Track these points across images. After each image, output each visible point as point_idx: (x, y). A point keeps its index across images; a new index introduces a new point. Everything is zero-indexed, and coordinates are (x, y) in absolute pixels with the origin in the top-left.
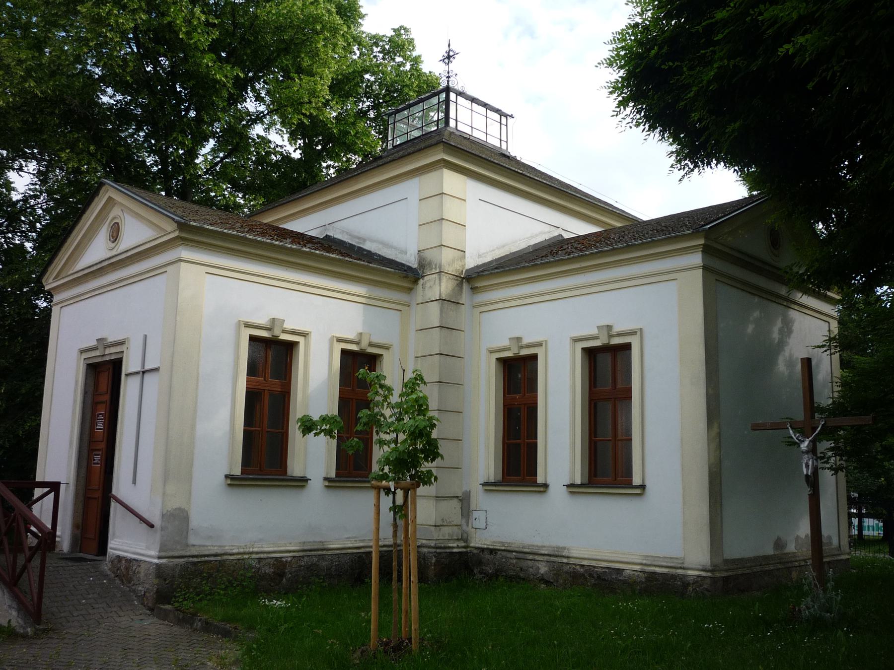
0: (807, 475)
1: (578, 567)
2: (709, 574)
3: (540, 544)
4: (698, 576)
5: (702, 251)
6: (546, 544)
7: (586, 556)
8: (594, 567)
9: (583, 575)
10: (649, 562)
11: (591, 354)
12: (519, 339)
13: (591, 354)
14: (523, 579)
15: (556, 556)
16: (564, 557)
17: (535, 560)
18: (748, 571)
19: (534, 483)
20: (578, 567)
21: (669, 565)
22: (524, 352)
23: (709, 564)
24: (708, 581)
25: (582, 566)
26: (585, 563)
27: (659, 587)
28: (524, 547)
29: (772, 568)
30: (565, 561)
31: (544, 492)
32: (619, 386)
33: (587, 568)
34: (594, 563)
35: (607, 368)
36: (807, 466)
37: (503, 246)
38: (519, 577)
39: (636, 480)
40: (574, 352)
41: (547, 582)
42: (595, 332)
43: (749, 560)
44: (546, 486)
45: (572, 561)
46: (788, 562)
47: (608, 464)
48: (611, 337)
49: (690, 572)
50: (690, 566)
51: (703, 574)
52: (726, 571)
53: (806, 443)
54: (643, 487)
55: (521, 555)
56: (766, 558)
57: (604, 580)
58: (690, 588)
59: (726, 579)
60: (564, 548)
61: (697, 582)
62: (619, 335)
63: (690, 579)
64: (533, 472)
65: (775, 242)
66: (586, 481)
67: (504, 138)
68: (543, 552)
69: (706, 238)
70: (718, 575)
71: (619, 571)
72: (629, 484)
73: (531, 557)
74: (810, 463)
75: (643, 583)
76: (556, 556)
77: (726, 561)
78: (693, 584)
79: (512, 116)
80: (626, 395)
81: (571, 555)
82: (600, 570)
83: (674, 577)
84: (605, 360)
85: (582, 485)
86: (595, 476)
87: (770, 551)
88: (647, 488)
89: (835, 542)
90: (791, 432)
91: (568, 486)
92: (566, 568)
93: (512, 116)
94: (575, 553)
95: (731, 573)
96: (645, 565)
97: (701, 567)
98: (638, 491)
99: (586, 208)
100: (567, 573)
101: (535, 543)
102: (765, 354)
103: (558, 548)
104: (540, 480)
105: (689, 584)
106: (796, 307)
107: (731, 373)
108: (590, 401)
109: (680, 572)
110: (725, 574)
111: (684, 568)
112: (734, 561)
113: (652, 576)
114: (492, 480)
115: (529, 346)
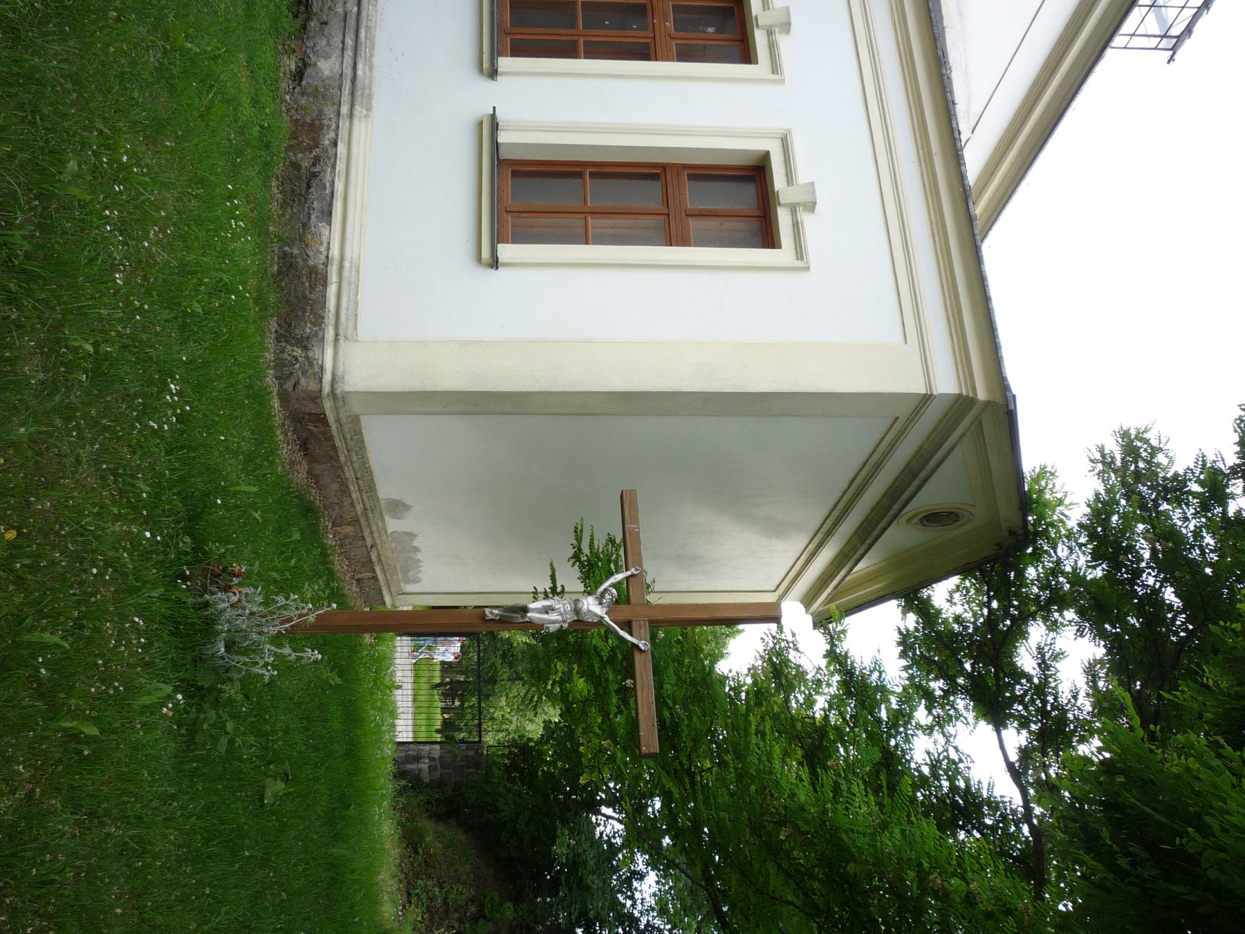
0: (524, 610)
1: (332, 135)
2: (326, 389)
3: (376, 61)
4: (322, 368)
5: (960, 395)
6: (377, 73)
7: (354, 151)
8: (334, 167)
9: (317, 145)
10: (346, 273)
11: (756, 173)
12: (786, 27)
13: (756, 173)
14: (304, 27)
15: (353, 93)
16: (352, 106)
17: (343, 50)
18: (342, 458)
19: (496, 52)
20: (332, 135)
21: (343, 312)
22: (760, 38)
23: (348, 388)
24: (313, 386)
25: (335, 144)
26: (341, 148)
27: (297, 294)
28: (368, 29)
29: (354, 496)
30: (345, 109)
31: (481, 71)
32: (693, 224)
33: (331, 152)
34: (340, 166)
35: (738, 200)
36: (547, 610)
37: (960, 13)
38: (308, 19)
39: (507, 251)
40: (761, 135)
41: (299, 75)
42: (802, 177)
43: (364, 460)
44: (493, 73)
45: (344, 124)
46: (367, 519)
47: (538, 195)
48: (793, 209)
49: (329, 352)
50: (341, 353)
51: (327, 378)
52: (338, 420)
53: (599, 610)
54: (495, 263)
55: (352, 22)
56: (371, 488)
57: (309, 187)
58: (298, 352)
59: (321, 419)
60: (369, 109)
61: (311, 365)
62: (796, 225)
63: (315, 353)
64: (519, 50)
65: (933, 518)
66: (504, 155)
67: (1136, 42)
68: (360, 66)
69: (988, 403)
70: (328, 405)
71: (327, 215)
72: (499, 237)
73: (349, 42)
74: (554, 616)
75: (305, 261)
76: (353, 93)
77: (356, 420)
78: (307, 357)
79: (1171, 59)
80: (675, 237)
81: (356, 121)
82: (328, 177)
83: (319, 320)
84: (743, 197)
85: (495, 146)
86: (515, 174)
87: (385, 491)
88: (493, 271)
89: (410, 588)
90: (619, 577)
91: (493, 117)
92: (329, 112)
93: (1171, 59)
94: (360, 128)
95: (334, 427)
96: (341, 267)
97: (339, 373)
98: (486, 254)
99: (998, 189)
100: (320, 113)
101: (377, 50)
102: (732, 493)
103: (370, 97)
104: (505, 63)
105: (305, 348)
106: (812, 546)
107: (714, 437)
108: (664, 167)
109: (330, 333)
110: (331, 418)
111: (336, 340)
112: (358, 432)
113: (318, 278)
114: (503, 138)
115: (772, 47)
